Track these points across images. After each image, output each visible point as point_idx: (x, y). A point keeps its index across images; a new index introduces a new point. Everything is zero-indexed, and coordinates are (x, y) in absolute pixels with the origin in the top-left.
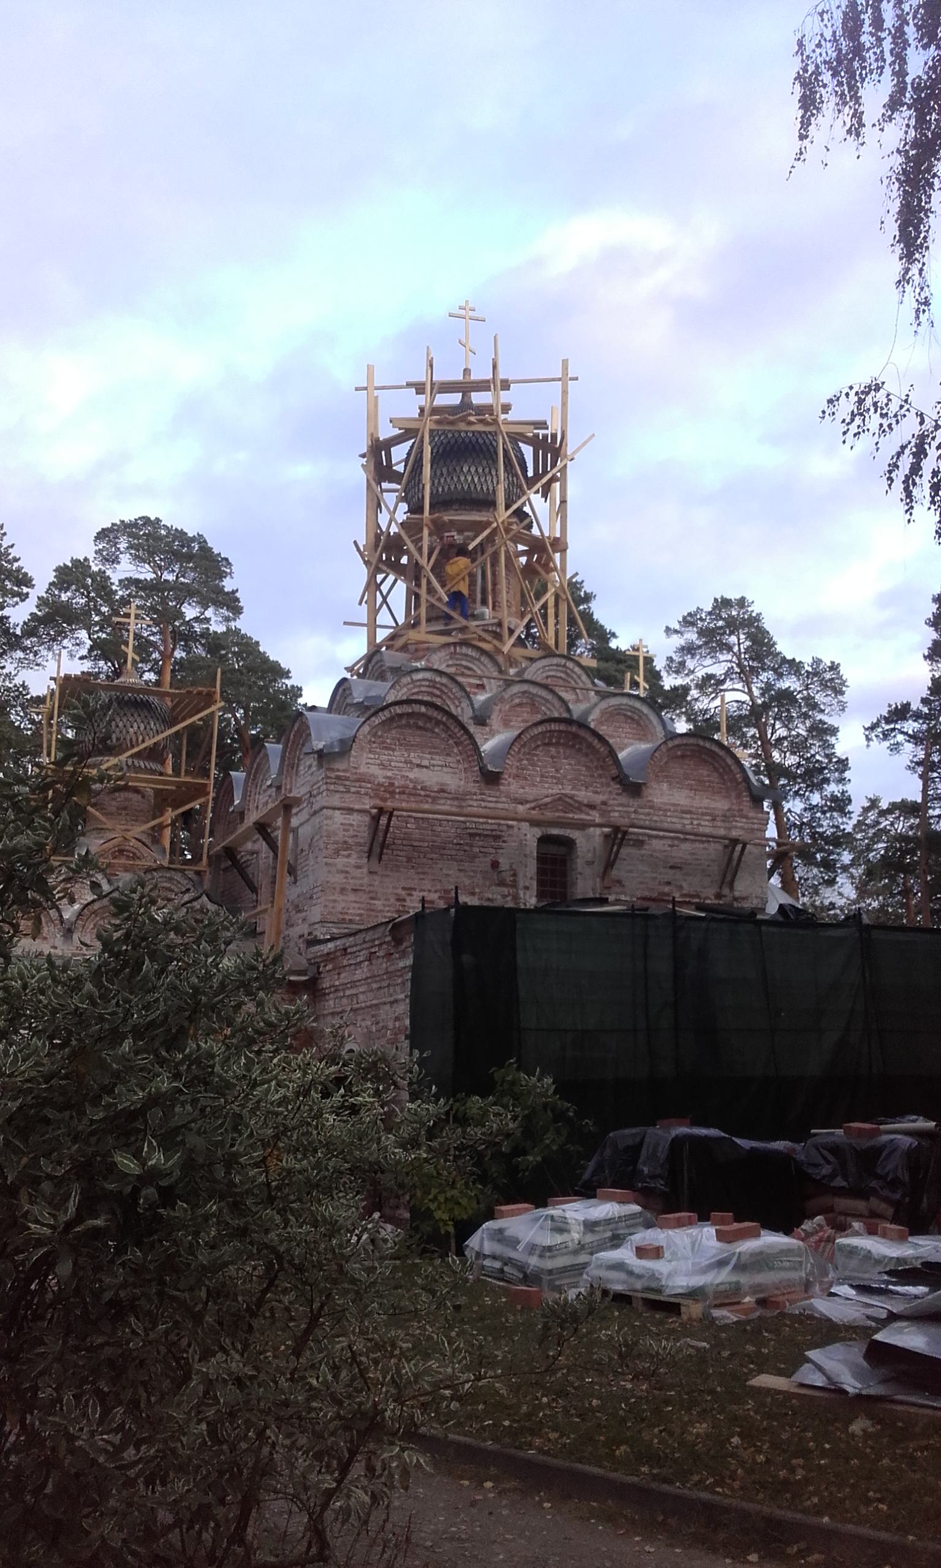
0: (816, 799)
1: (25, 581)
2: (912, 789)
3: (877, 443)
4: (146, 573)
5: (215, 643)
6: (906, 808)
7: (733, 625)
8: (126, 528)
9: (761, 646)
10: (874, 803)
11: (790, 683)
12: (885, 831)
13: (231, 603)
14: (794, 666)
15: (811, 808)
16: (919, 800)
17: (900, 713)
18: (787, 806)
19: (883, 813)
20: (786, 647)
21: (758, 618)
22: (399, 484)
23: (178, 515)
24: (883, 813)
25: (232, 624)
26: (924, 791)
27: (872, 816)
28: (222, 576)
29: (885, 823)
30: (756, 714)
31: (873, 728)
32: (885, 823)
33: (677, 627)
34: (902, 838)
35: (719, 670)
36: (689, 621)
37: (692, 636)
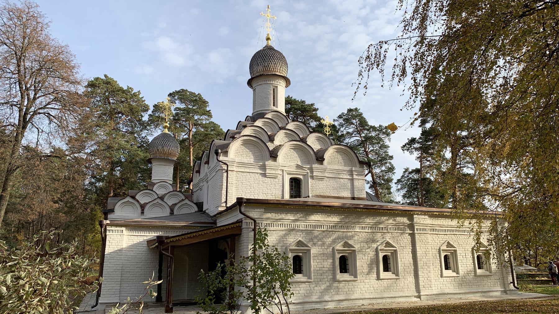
0: (383, 168)
1: (246, 143)
2: (417, 165)
3: (355, 93)
4: (183, 106)
5: (205, 127)
6: (417, 171)
7: (354, 117)
8: (178, 92)
9: (363, 123)
10: (406, 170)
11: (373, 134)
12: (410, 178)
13: (209, 114)
14: (374, 128)
15: (382, 171)
16: (419, 167)
17: (413, 141)
18: (374, 171)
19: (410, 173)
20: (371, 123)
21: (361, 114)
22: (291, 196)
23: (194, 88)
24: (410, 173)
25: (211, 120)
26: (421, 165)
27: (407, 174)
28: (206, 107)
29: (410, 176)
30: (363, 143)
31: (404, 146)
32: (410, 176)
33: (337, 119)
34: (415, 180)
35: (351, 130)
36: (340, 117)
37: (341, 121)
